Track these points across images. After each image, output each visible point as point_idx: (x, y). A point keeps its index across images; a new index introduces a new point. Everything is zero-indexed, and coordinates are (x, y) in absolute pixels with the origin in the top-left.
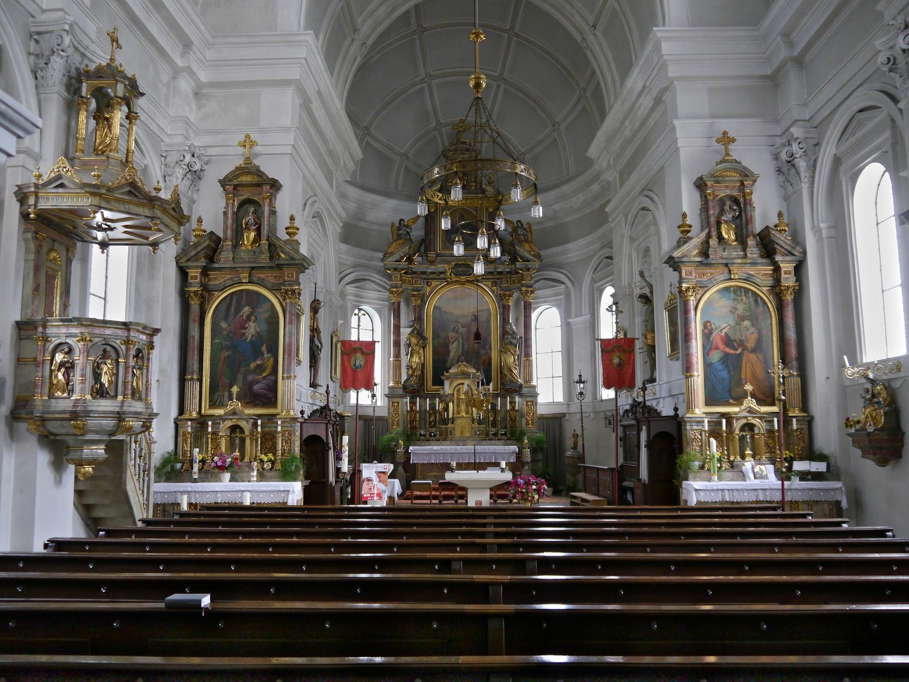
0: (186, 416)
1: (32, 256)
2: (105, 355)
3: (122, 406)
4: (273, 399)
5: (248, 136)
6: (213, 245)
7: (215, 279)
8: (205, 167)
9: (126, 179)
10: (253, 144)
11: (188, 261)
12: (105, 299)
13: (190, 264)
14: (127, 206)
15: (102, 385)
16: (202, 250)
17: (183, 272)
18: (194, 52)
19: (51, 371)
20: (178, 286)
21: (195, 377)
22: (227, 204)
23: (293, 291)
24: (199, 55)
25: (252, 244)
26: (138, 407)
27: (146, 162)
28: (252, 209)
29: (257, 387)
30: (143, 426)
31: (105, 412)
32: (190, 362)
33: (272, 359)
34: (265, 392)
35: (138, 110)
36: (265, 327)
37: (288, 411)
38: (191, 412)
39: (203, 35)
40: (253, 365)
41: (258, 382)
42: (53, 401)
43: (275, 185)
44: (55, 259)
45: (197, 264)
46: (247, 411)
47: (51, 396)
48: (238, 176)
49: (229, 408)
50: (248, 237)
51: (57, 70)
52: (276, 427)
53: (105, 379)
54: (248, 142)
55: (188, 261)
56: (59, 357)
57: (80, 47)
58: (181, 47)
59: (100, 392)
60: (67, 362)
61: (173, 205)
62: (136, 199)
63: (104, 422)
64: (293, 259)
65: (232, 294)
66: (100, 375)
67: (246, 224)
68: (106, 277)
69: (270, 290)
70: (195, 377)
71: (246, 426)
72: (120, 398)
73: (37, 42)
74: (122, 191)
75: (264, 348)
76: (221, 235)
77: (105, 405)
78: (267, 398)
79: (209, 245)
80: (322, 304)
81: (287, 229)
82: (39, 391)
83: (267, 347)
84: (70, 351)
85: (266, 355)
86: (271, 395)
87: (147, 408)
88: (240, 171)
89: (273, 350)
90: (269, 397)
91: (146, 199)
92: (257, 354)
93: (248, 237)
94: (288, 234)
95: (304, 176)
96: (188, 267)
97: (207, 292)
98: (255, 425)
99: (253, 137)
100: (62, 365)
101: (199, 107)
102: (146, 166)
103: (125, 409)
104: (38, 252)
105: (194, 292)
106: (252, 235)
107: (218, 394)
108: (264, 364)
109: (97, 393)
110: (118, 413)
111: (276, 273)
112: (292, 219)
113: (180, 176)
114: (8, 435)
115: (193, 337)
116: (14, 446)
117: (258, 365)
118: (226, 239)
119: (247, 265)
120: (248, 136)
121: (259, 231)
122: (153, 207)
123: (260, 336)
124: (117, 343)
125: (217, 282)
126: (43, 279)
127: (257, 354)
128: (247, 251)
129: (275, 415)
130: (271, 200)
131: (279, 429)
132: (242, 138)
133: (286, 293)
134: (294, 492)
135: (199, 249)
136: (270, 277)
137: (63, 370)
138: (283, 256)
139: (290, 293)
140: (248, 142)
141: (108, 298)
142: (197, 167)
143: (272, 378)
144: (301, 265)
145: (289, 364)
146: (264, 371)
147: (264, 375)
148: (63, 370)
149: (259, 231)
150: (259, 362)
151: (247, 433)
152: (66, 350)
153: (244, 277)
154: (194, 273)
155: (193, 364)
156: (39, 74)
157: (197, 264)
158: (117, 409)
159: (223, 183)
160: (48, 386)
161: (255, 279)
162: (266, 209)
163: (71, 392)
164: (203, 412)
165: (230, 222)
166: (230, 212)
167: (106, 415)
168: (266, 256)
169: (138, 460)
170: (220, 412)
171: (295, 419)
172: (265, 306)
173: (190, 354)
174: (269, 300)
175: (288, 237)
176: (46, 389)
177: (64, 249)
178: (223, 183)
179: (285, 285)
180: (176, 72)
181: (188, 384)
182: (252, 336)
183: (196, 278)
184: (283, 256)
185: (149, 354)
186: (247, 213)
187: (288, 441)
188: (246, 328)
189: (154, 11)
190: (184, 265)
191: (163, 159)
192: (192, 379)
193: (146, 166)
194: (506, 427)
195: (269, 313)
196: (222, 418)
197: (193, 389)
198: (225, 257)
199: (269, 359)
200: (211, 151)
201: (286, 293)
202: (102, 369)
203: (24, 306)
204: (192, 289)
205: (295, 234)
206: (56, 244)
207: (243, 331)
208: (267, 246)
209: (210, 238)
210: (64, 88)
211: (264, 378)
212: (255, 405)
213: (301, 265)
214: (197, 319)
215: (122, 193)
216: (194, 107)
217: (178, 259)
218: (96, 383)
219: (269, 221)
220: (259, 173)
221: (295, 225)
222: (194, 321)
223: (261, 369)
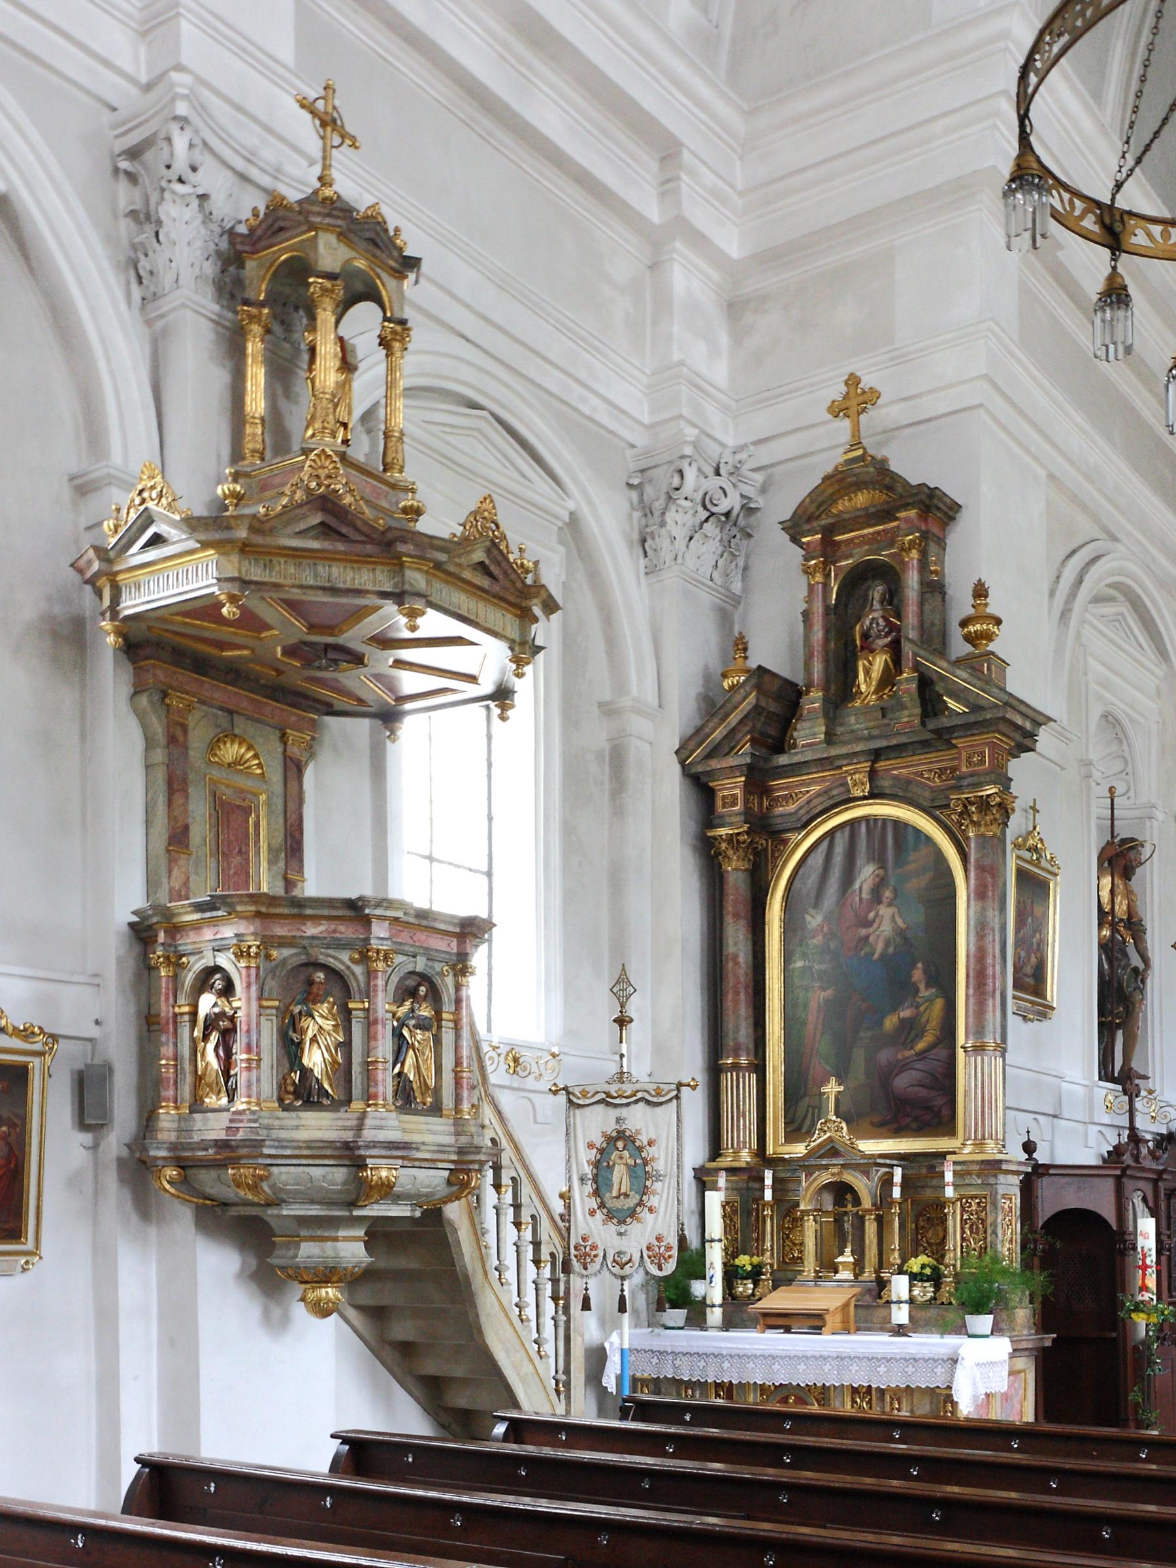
0: (726, 1161)
1: (159, 756)
2: (310, 996)
3: (359, 1128)
4: (945, 1112)
5: (853, 381)
6: (773, 707)
7: (785, 798)
8: (759, 502)
9: (308, 490)
10: (869, 398)
11: (709, 756)
12: (489, 874)
13: (715, 764)
14: (322, 570)
15: (306, 1072)
16: (741, 722)
17: (701, 786)
18: (693, 174)
19: (193, 1041)
20: (693, 826)
21: (743, 1061)
22: (811, 587)
23: (984, 804)
24: (709, 178)
25: (876, 692)
26: (431, 1132)
27: (571, 505)
28: (877, 591)
29: (902, 1082)
30: (449, 1182)
31: (309, 1144)
32: (730, 1023)
33: (939, 1003)
34: (923, 1093)
35: (408, 313)
36: (917, 916)
37: (980, 1144)
38: (736, 1152)
39: (712, 115)
40: (890, 1022)
41: (903, 1067)
42: (197, 1116)
43: (936, 510)
44: (239, 761)
45: (731, 761)
46: (870, 1146)
47: (197, 1105)
48: (833, 499)
49: (819, 1139)
50: (867, 672)
51: (186, 250)
52: (943, 1187)
53: (315, 1059)
54: (856, 400)
55: (709, 756)
56: (207, 1003)
57: (254, 173)
58: (655, 166)
59: (302, 1092)
60: (222, 1015)
61: (479, 555)
62: (341, 547)
63: (317, 1172)
64: (976, 708)
65: (831, 833)
66: (299, 1045)
67: (865, 636)
68: (490, 819)
69: (928, 811)
70: (743, 1061)
71: (865, 1186)
72: (357, 1105)
73: (132, 177)
74: (302, 526)
75: (918, 975)
76: (799, 679)
77: (318, 1126)
78: (929, 1108)
79: (757, 708)
80: (1146, 852)
81: (964, 624)
82: (171, 1093)
83: (925, 972)
84: (228, 990)
85: (924, 993)
86: (939, 1101)
87: (457, 1134)
88: (840, 482)
89: (944, 982)
90: (928, 1105)
91: (370, 540)
92: (901, 990)
93: (867, 672)
94: (970, 639)
95: (1051, 476)
96: (710, 773)
97: (766, 837)
98: (887, 1182)
99: (867, 382)
100: (210, 1024)
101: (738, 336)
102: (571, 514)
103: (368, 1135)
104: (176, 739)
105: (730, 839)
106: (879, 662)
107: (805, 1102)
108: (919, 1015)
109: (297, 1095)
110: (347, 1145)
111: (938, 759)
112: (980, 591)
113: (681, 533)
114: (129, 1206)
115: (736, 957)
116: (153, 1231)
117: (903, 1021)
118: (809, 685)
119: (859, 747)
120: (853, 381)
121: (895, 649)
122: (397, 565)
123: (906, 940)
124: (342, 959)
125: (791, 808)
126: (199, 812)
127: (901, 990)
128: (867, 710)
129: (942, 1156)
130: (924, 553)
131: (949, 1192)
132: (837, 390)
133: (966, 813)
134: (986, 1371)
135: (734, 719)
136: (920, 768)
137: (214, 1037)
138: (952, 704)
139: (980, 811)
140: (856, 400)
141: (494, 870)
142: (731, 502)
143: (942, 1053)
144: (1019, 730)
145: (993, 1017)
146: (920, 1035)
147: (921, 1046)
148: (214, 1037)
149: (895, 649)
150: (906, 1013)
151: (867, 1203)
152: (219, 985)
153: (857, 780)
154: (732, 787)
155: (740, 1029)
156: (144, 265)
157: (731, 761)
158: (349, 1136)
159: (794, 528)
160: (189, 1079)
161: (885, 784)
162: (912, 580)
163: (231, 1095)
164: (770, 1150)
165: (818, 634)
166: (818, 608)
167: (317, 1152)
168: (909, 715)
169: (530, 1270)
170: (799, 1150)
171: (994, 1167)
172: (917, 858)
173: (729, 1003)
174: (929, 839)
175: (969, 648)
176: (186, 1091)
177: (274, 736)
178: (794, 528)
179: (958, 788)
180: (656, 247)
181: (727, 1079)
182: (887, 944)
183: (734, 804)
184: (952, 704)
185: (458, 987)
186: (865, 602)
187: (979, 1225)
188: (869, 924)
189: (536, 63)
190: (700, 769)
191: (634, 495)
192: (736, 1067)
193: (571, 514)
194: (249, 1096)
195: (930, 874)
196: (805, 1165)
197: (740, 1091)
198: (809, 734)
199: (930, 1000)
200: (764, 456)
201: (966, 813)
202: (303, 1032)
203: (151, 884)
204: (723, 831)
205: (989, 637)
206: (236, 717)
207: (863, 932)
208: (914, 686)
209: (758, 687)
210: (210, 290)
211: (922, 1056)
212: (898, 1131)
213: (1019, 730)
214: (743, 910)
215: (300, 534)
216: (724, 339)
217: (682, 753)
218: (292, 1070)
219: (921, 613)
220: (882, 477)
221: (990, 610)
222: (736, 916)
223: (910, 1030)
